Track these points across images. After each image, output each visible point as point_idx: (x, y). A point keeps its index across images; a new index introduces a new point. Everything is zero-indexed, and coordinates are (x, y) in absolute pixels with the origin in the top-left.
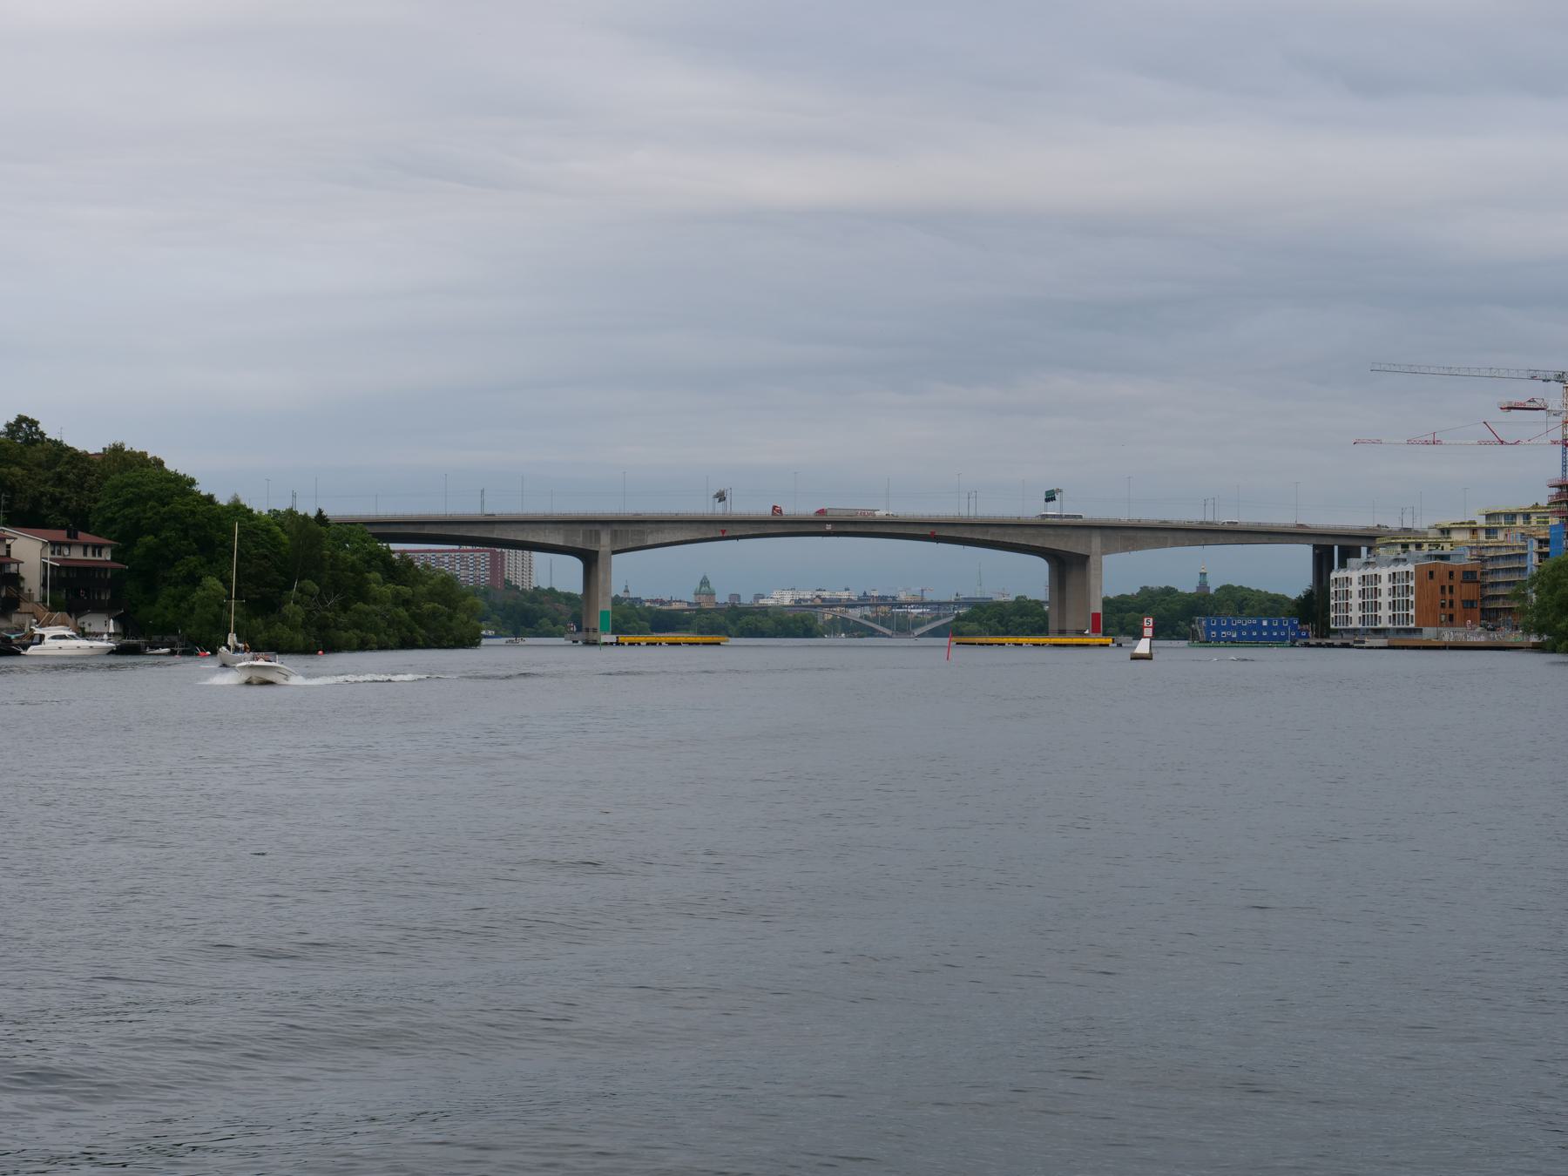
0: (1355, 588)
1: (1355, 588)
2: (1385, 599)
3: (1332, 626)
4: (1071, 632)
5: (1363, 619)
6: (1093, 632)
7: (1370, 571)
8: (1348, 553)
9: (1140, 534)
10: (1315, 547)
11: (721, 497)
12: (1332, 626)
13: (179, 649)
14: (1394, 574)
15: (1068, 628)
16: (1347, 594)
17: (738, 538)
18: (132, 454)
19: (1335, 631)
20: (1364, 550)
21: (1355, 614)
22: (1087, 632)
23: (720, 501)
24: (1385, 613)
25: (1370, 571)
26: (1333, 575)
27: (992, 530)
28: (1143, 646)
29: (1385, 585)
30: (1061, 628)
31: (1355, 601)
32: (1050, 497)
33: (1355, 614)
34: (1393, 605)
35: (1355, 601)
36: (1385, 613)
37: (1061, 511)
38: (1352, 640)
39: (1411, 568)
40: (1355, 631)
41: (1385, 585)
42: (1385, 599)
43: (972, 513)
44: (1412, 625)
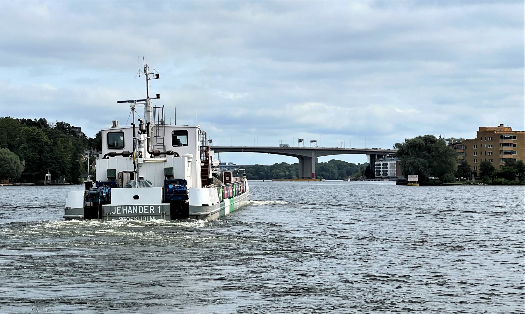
0: (381, 166)
1: (381, 166)
2: (389, 169)
3: (376, 176)
4: (306, 178)
5: (391, 174)
6: (313, 178)
7: (385, 162)
8: (380, 156)
9: (325, 151)
10: (370, 155)
11: (300, 141)
12: (376, 176)
13: (72, 183)
14: (391, 163)
15: (305, 177)
16: (380, 168)
17: (268, 153)
18: (458, 140)
19: (376, 177)
20: (384, 156)
21: (381, 173)
22: (311, 178)
23: (210, 142)
24: (389, 173)
25: (385, 162)
26: (376, 163)
27: (286, 151)
28: (349, 180)
29: (389, 166)
30: (303, 177)
31: (381, 170)
32: (300, 141)
33: (381, 173)
34: (390, 171)
35: (381, 170)
36: (389, 173)
37: (299, 146)
38: (381, 179)
39: (395, 162)
40: (381, 177)
41: (389, 166)
42: (389, 169)
43: (216, 146)
44: (395, 176)
